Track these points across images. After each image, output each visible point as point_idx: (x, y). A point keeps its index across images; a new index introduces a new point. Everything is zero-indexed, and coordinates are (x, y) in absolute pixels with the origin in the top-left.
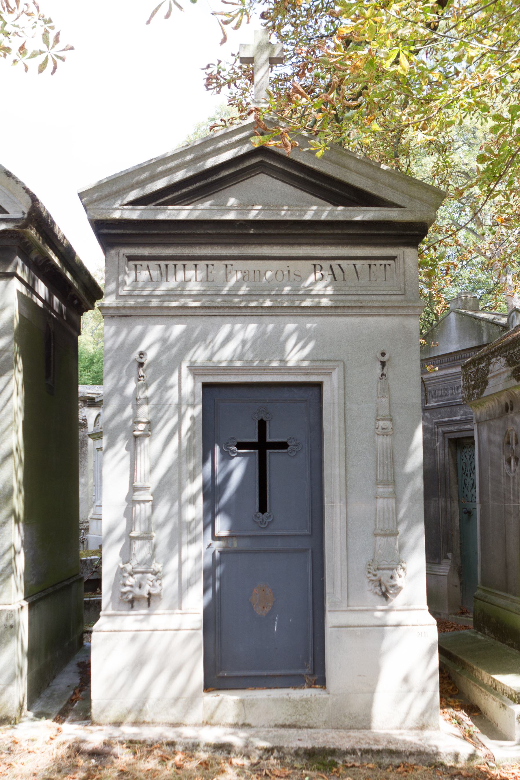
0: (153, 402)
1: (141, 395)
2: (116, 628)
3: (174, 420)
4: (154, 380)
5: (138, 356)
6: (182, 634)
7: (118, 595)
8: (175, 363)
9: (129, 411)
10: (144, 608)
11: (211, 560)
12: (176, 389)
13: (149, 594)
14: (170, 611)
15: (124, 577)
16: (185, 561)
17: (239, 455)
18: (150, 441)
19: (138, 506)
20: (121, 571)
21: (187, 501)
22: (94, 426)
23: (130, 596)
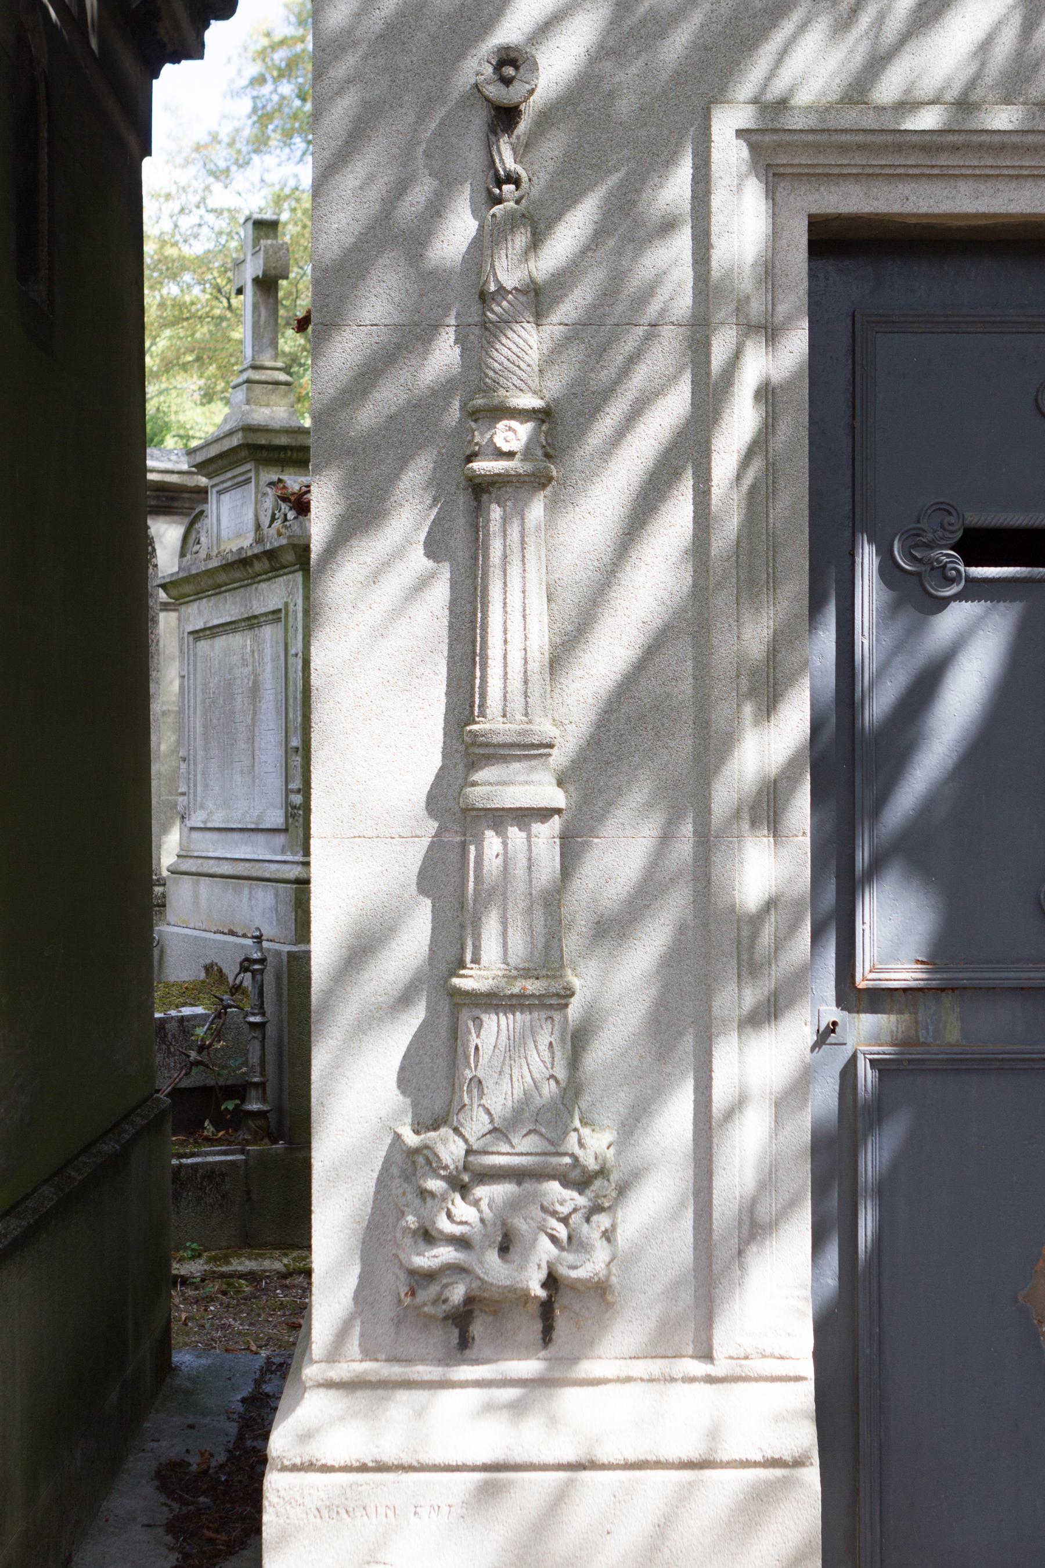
0: (569, 308)
1: (508, 272)
2: (390, 1451)
3: (674, 406)
4: (569, 200)
5: (489, 70)
6: (725, 1487)
7: (396, 1283)
8: (680, 116)
9: (445, 355)
10: (521, 1352)
11: (834, 1102)
12: (683, 241)
13: (552, 1282)
14: (655, 1367)
15: (424, 1194)
16: (729, 1115)
17: (976, 590)
18: (553, 507)
19: (492, 842)
20: (405, 1169)
21: (737, 815)
22: (182, 554)
23: (458, 1293)
